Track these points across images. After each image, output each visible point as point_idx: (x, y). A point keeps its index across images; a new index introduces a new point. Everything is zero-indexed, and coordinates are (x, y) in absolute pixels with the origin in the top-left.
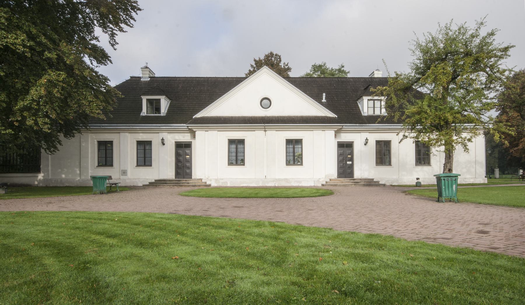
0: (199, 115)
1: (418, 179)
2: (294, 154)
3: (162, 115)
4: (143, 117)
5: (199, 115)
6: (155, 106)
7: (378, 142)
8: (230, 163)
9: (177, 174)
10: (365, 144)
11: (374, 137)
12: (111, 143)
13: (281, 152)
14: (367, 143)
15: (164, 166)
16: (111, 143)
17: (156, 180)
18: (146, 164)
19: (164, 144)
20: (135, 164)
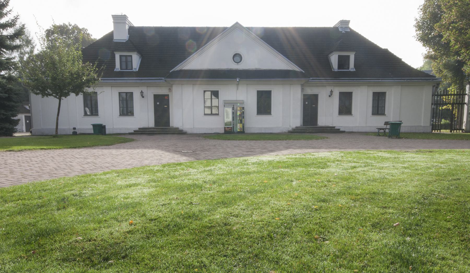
0: (178, 68)
1: (74, 129)
2: (264, 105)
3: (134, 70)
4: (116, 72)
5: (178, 68)
6: (126, 61)
7: (341, 94)
8: (373, 114)
9: (157, 122)
10: (330, 96)
11: (150, 92)
12: (132, 93)
13: (336, 102)
14: (331, 94)
15: (144, 116)
16: (132, 93)
17: (139, 129)
18: (379, 113)
19: (143, 97)
20: (119, 114)
